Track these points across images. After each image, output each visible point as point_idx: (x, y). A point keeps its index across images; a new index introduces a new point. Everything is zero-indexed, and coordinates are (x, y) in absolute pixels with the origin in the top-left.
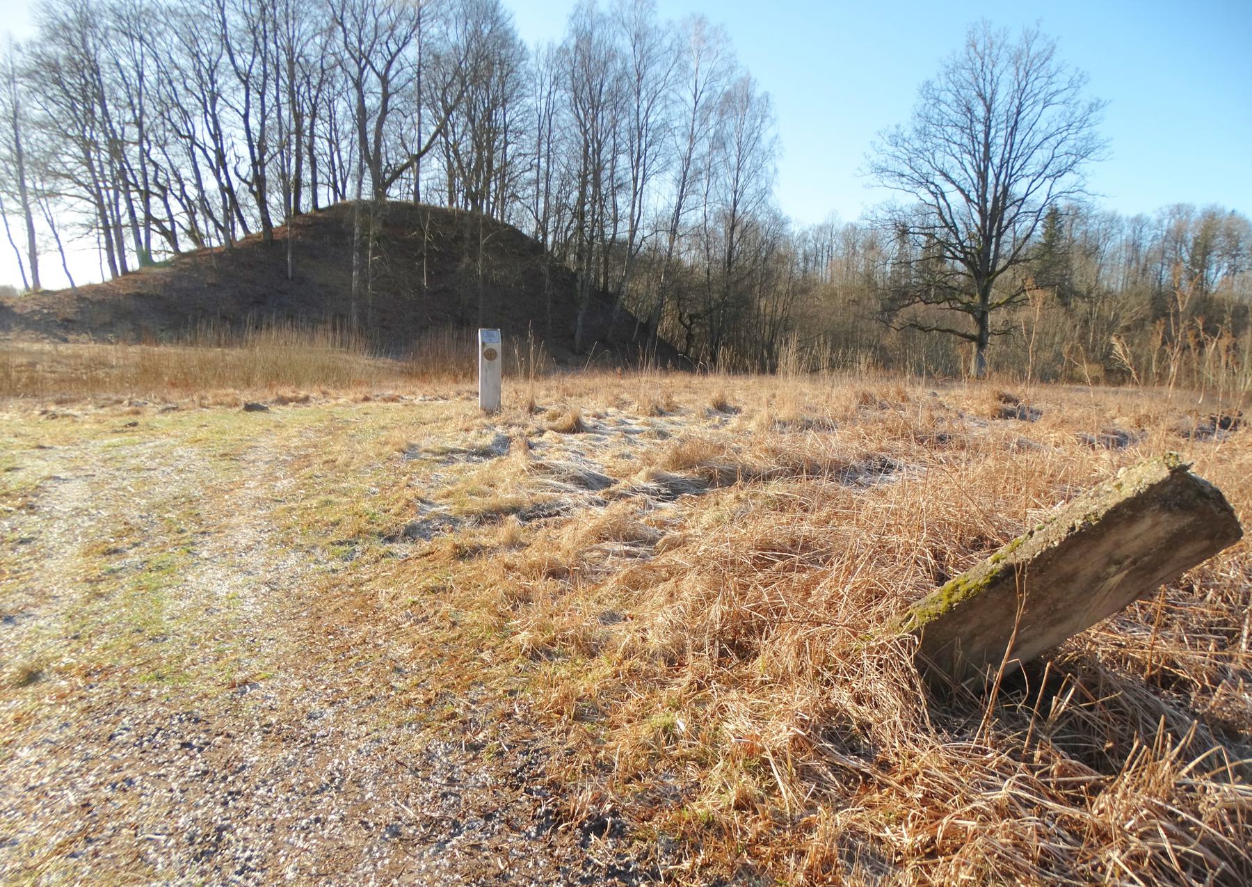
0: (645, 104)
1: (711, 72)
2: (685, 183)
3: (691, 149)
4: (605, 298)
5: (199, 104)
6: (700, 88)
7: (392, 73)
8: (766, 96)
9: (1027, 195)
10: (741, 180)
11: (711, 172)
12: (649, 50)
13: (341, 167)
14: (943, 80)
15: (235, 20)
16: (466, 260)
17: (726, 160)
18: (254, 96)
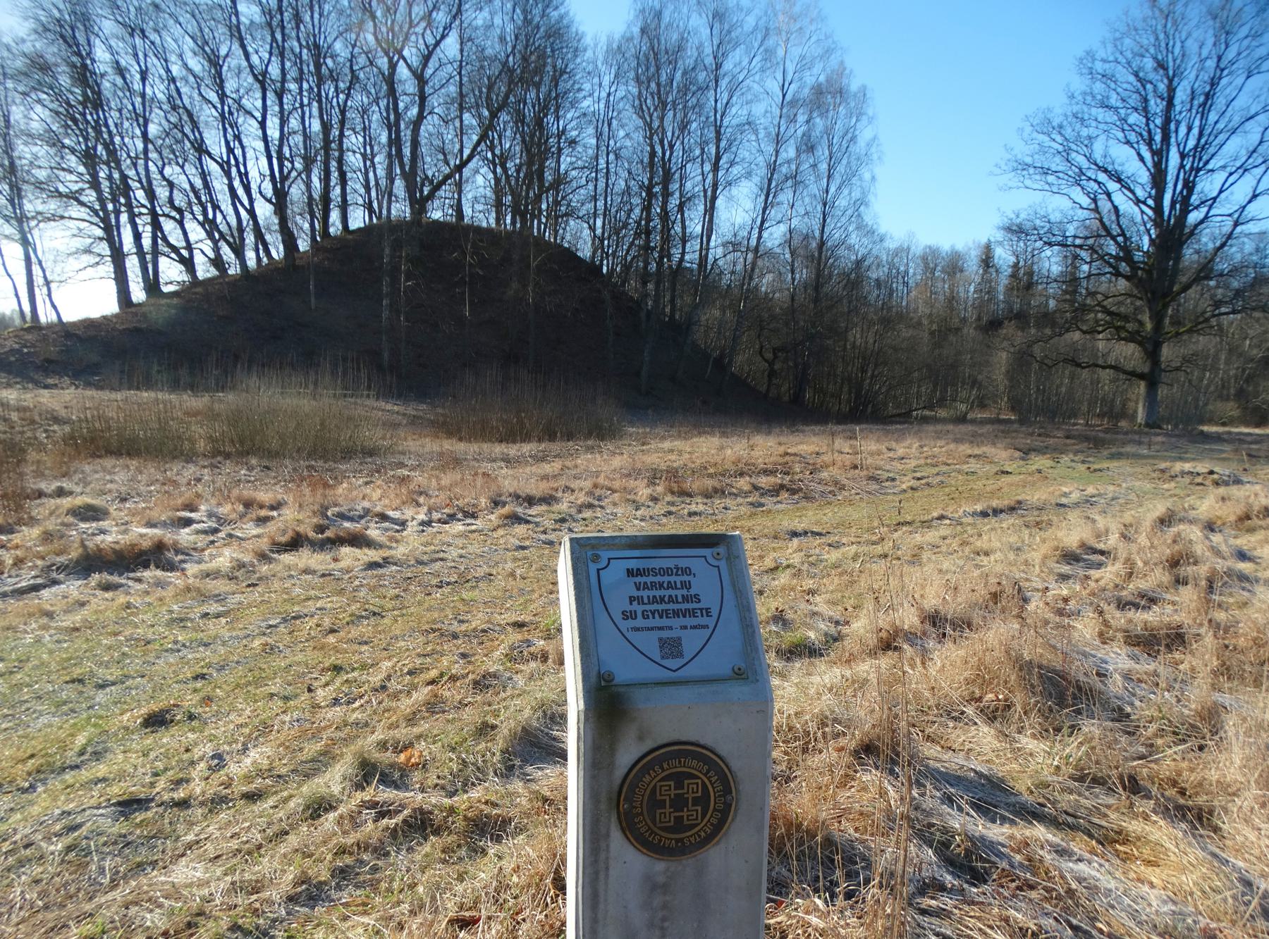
0: (725, 96)
1: (802, 57)
2: (769, 193)
3: (777, 152)
4: (678, 330)
5: (216, 114)
6: (789, 78)
7: (429, 72)
8: (863, 90)
9: (1221, 192)
10: (832, 189)
11: (795, 180)
12: (729, 32)
13: (377, 184)
14: (1110, 48)
15: (249, 12)
16: (515, 285)
17: (814, 166)
18: (271, 96)
